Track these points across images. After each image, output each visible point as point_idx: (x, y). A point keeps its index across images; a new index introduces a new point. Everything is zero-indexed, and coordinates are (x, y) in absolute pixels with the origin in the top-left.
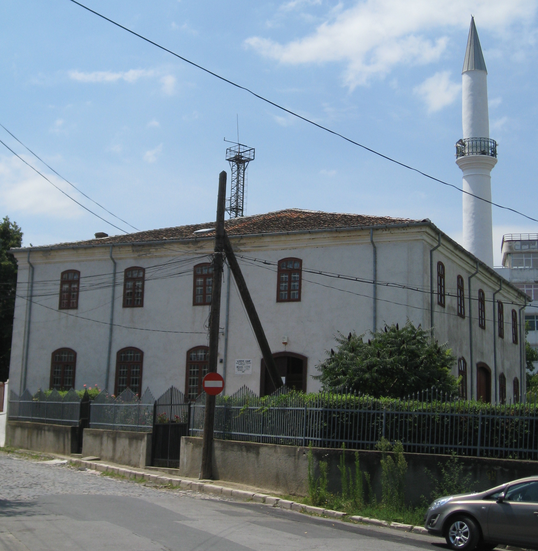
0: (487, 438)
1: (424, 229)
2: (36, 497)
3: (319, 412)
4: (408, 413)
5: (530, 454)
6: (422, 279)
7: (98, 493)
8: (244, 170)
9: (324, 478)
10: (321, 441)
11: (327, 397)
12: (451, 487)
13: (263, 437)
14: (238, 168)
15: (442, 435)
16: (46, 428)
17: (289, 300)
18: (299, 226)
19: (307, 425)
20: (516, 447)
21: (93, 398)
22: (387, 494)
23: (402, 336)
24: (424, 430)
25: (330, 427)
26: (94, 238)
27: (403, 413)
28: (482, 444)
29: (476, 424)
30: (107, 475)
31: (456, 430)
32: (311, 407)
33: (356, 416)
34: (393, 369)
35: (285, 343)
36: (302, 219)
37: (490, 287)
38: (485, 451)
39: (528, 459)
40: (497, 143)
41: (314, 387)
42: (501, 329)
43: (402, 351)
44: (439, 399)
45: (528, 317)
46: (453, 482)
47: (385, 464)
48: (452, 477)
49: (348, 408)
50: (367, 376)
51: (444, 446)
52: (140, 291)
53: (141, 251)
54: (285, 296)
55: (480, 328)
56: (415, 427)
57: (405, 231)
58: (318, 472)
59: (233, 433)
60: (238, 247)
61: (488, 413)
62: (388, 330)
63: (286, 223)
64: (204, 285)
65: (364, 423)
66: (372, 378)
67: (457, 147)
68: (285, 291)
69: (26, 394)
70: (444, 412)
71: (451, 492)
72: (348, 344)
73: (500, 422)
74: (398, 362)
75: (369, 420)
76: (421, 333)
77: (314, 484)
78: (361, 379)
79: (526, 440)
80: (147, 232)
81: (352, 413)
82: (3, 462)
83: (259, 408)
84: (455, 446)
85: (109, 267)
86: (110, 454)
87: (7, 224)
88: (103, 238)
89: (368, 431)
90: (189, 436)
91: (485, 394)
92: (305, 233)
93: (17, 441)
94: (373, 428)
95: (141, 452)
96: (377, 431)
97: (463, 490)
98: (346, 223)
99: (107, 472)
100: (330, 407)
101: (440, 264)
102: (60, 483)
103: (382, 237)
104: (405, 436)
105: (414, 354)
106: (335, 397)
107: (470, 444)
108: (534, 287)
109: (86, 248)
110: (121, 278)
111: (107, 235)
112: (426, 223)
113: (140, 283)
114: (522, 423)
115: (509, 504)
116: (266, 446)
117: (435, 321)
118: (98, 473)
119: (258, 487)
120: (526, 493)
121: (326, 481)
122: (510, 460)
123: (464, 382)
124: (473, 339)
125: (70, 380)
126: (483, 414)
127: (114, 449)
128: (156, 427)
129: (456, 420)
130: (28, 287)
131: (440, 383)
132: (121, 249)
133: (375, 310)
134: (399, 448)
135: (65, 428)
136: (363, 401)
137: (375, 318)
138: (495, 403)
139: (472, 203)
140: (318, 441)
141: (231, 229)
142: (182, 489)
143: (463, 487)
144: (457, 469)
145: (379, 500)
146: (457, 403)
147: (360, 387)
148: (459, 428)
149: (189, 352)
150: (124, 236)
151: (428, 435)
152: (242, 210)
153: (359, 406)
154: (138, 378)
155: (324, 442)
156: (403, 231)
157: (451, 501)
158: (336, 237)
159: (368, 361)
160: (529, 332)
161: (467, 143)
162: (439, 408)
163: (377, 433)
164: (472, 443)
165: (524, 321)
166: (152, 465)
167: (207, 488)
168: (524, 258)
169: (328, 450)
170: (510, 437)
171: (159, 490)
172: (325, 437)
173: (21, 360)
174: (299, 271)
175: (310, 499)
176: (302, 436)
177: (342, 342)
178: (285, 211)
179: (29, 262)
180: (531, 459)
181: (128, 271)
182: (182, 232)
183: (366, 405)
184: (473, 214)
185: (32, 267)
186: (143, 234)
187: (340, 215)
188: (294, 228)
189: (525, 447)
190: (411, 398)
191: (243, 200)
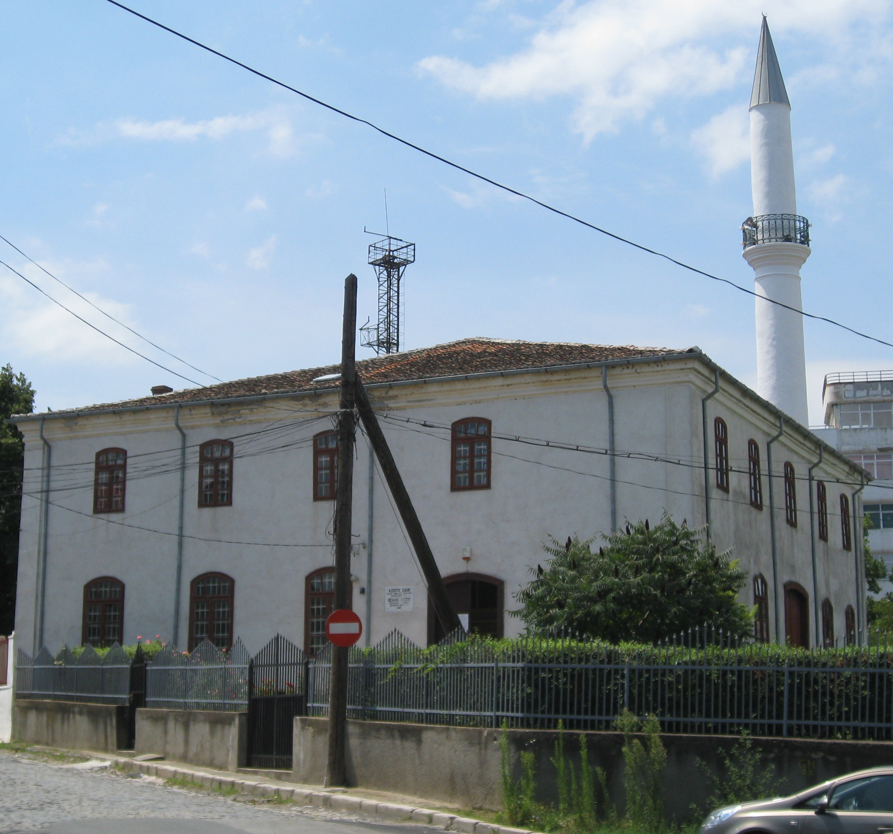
0: (799, 706)
1: (690, 365)
2: (45, 825)
3: (518, 671)
4: (667, 667)
5: (871, 730)
6: (690, 445)
7: (152, 815)
8: (399, 280)
9: (528, 780)
10: (522, 718)
11: (530, 644)
12: (740, 789)
13: (427, 714)
14: (389, 276)
15: (724, 702)
16: (77, 709)
17: (472, 487)
18: (485, 365)
19: (498, 692)
20: (848, 719)
21: (151, 658)
22: (634, 803)
23: (655, 540)
24: (693, 696)
25: (536, 693)
26: (150, 394)
27: (657, 667)
28: (790, 717)
29: (780, 683)
30: (174, 783)
31: (747, 695)
32: (504, 662)
33: (580, 675)
34: (642, 595)
35: (467, 559)
36: (490, 354)
37: (803, 457)
38: (795, 727)
39: (869, 738)
40: (809, 223)
41: (514, 628)
42: (823, 525)
43: (656, 564)
44: (717, 643)
45: (867, 507)
46: (744, 780)
47: (630, 753)
48: (742, 772)
49: (566, 662)
50: (598, 608)
51: (728, 720)
52: (226, 479)
53: (226, 413)
54: (465, 482)
55: (789, 527)
56: (678, 691)
57: (659, 368)
58: (518, 769)
59: (378, 708)
60: (386, 402)
61: (800, 663)
62: (632, 532)
63: (465, 361)
64: (331, 467)
65: (594, 687)
66: (607, 610)
67: (744, 231)
68: (465, 472)
69: (44, 655)
70: (726, 665)
71: (741, 798)
72: (565, 556)
73: (820, 680)
74: (649, 584)
75: (601, 681)
76: (687, 535)
77: (513, 790)
78: (588, 614)
79: (863, 707)
80: (237, 383)
81: (574, 669)
82: (2, 767)
83: (420, 666)
84: (747, 721)
85: (175, 440)
86: (180, 749)
87: (8, 377)
88: (164, 395)
89: (601, 699)
90: (307, 715)
91: (799, 634)
92: (494, 377)
93: (31, 732)
94: (608, 695)
95: (230, 743)
96: (615, 699)
97: (760, 793)
98: (562, 358)
99: (174, 779)
100: (536, 661)
101: (719, 421)
102: (92, 800)
103: (622, 380)
104: (663, 706)
105: (676, 571)
106: (544, 645)
107: (770, 717)
108: (878, 457)
109: (135, 412)
110: (193, 458)
111: (171, 390)
112: (694, 355)
113: (226, 467)
114: (857, 679)
115: (836, 817)
116: (431, 729)
117: (712, 516)
118: (160, 781)
119: (422, 797)
120: (864, 797)
121: (532, 785)
122: (837, 741)
123: (762, 615)
124: (777, 545)
125: (114, 629)
126: (791, 666)
127: (187, 742)
128: (254, 703)
129: (747, 677)
130: (42, 477)
131: (720, 615)
132: (193, 412)
133: (613, 501)
134: (654, 726)
135: (107, 708)
136: (591, 649)
137: (614, 513)
138: (816, 649)
139: (771, 322)
140: (517, 718)
141: (373, 372)
142: (296, 803)
143: (761, 788)
144: (750, 760)
145: (621, 814)
146: (748, 648)
147: (584, 626)
148: (751, 691)
149: (309, 578)
150: (199, 390)
151: (700, 704)
152: (397, 345)
153: (584, 657)
154: (226, 622)
155: (528, 719)
156: (656, 369)
157: (738, 812)
158: (547, 381)
159: (599, 583)
160: (869, 531)
161: (760, 224)
162: (719, 657)
163: (616, 703)
164: (774, 714)
165: (861, 512)
166: (249, 765)
167: (337, 801)
168: (860, 412)
169: (534, 733)
170: (837, 703)
171: (257, 808)
172: (529, 710)
173: (33, 599)
174: (487, 438)
175: (506, 816)
176: (492, 710)
177: (557, 553)
178: (463, 342)
179: (42, 437)
180: (874, 739)
181: (205, 447)
182: (295, 380)
183: (595, 656)
184: (774, 339)
185: (48, 446)
186: (230, 385)
187: (552, 345)
188: (477, 369)
189: (863, 718)
190: (671, 642)
191: (398, 329)
